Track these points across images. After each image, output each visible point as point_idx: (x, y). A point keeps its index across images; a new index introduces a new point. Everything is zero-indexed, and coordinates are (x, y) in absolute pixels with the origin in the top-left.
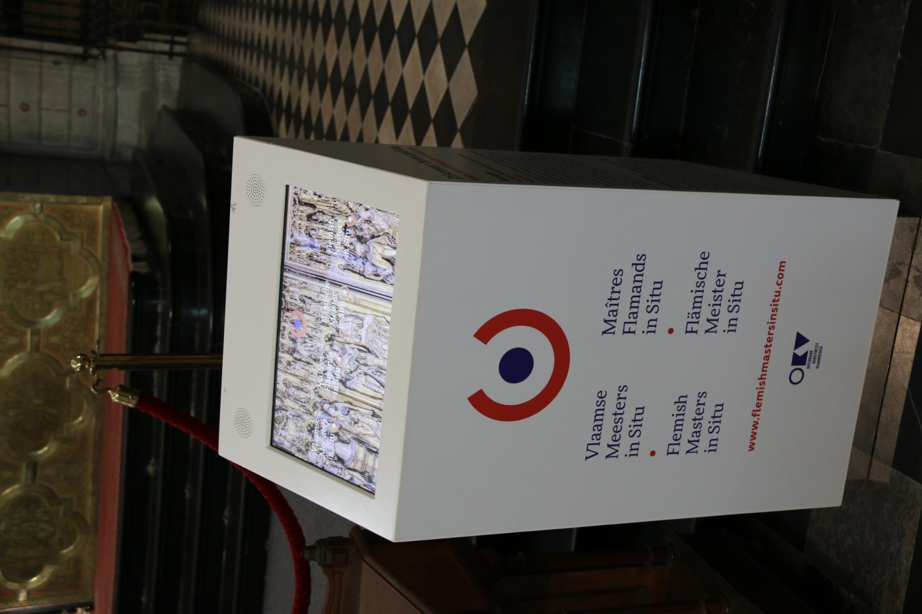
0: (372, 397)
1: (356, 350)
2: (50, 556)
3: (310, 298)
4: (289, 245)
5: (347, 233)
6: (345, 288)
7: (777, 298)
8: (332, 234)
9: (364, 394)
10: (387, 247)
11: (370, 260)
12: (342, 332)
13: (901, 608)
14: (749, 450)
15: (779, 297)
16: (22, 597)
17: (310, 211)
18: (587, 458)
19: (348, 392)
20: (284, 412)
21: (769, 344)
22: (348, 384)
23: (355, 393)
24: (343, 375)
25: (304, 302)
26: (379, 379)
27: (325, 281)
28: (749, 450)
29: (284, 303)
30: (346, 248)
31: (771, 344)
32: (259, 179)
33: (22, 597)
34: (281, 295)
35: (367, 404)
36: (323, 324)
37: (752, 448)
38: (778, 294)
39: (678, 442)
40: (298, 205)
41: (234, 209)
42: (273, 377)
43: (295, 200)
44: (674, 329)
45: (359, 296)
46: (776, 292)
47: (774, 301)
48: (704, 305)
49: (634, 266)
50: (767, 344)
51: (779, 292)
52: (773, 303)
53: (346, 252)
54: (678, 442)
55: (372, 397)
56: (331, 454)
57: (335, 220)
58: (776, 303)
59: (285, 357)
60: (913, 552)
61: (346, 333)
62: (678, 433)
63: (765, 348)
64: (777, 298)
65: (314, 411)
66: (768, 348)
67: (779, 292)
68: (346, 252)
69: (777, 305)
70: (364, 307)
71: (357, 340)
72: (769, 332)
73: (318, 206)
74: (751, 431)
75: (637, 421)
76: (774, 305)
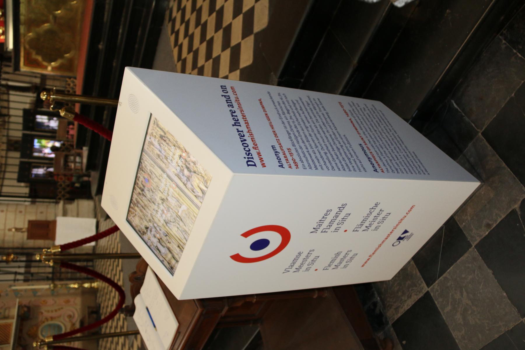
0: (179, 239)
1: (175, 215)
2: (62, 57)
3: (155, 174)
4: (148, 142)
5: (181, 160)
6: (174, 184)
8: (164, 193)
10: (202, 183)
11: (191, 181)
12: (169, 202)
13: (396, 319)
16: (49, 68)
17: (163, 134)
18: (283, 273)
19: (167, 227)
20: (134, 211)
22: (168, 224)
24: (166, 220)
25: (152, 174)
26: (184, 235)
27: (164, 173)
29: (141, 166)
30: (179, 166)
32: (133, 110)
33: (49, 68)
34: (140, 162)
36: (160, 190)
37: (363, 266)
40: (156, 126)
41: (120, 105)
42: (149, 117)
43: (154, 122)
45: (181, 193)
48: (368, 220)
49: (339, 208)
53: (178, 168)
55: (179, 239)
56: (155, 245)
57: (175, 149)
59: (138, 190)
60: (411, 306)
61: (172, 204)
68: (178, 168)
70: (183, 200)
73: (167, 134)
75: (313, 261)
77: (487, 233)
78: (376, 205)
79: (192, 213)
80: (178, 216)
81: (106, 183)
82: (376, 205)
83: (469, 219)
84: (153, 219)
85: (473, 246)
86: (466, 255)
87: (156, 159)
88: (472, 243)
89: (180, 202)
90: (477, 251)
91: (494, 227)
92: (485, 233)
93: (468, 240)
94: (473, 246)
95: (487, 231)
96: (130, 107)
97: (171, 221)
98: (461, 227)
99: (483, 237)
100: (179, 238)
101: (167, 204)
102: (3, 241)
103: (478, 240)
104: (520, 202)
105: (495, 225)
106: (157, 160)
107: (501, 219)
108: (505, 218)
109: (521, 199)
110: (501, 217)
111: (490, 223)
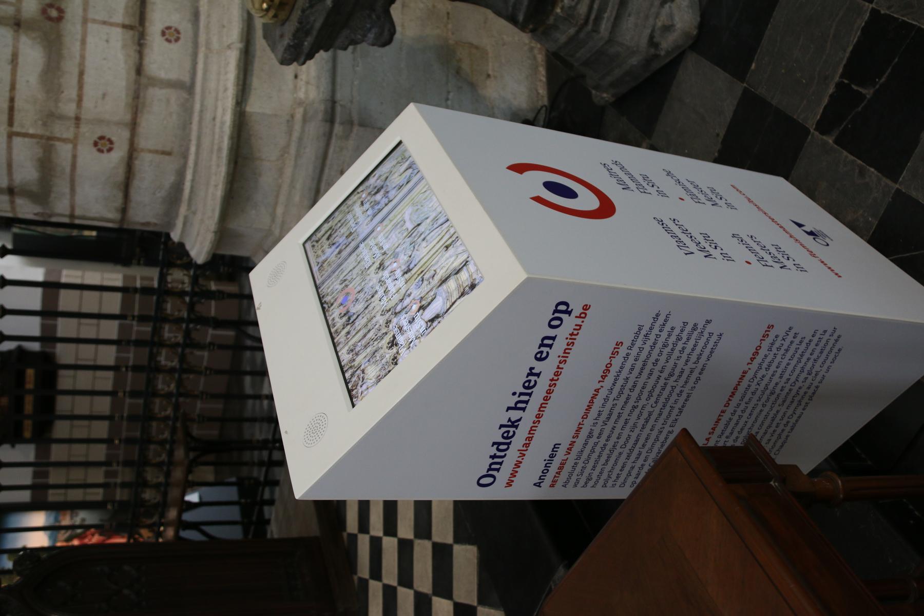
7: (575, 332)
9: (428, 253)
14: (506, 487)
15: (579, 331)
21: (556, 378)
23: (422, 261)
28: (506, 487)
31: (578, 333)
35: (437, 251)
38: (578, 327)
39: (529, 391)
44: (543, 181)
46: (576, 325)
47: (572, 334)
50: (553, 378)
51: (580, 326)
52: (569, 337)
54: (529, 391)
58: (573, 337)
62: (545, 349)
63: (550, 382)
64: (575, 332)
65: (434, 6)
66: (553, 382)
67: (580, 326)
69: (575, 339)
71: (340, 323)
72: (558, 366)
74: (508, 478)
76: (570, 339)
77: (872, 170)
78: (790, 328)
79: (421, 195)
80: (410, 234)
81: (286, 432)
82: (790, 328)
83: (861, 212)
84: (390, 310)
85: (897, 186)
86: (914, 194)
87: (341, 277)
88: (893, 191)
89: (398, 221)
90: (902, 176)
91: (861, 162)
92: (873, 173)
93: (890, 199)
94: (897, 186)
95: (869, 170)
96: (279, 278)
97: (410, 253)
98: (877, 222)
99: (879, 174)
100: (438, 239)
101: (390, 254)
102: (154, 3)
103: (885, 181)
104: (824, 137)
105: (859, 162)
106: (343, 257)
107: (849, 155)
108: (846, 150)
109: (820, 136)
110: (846, 157)
111: (857, 171)
